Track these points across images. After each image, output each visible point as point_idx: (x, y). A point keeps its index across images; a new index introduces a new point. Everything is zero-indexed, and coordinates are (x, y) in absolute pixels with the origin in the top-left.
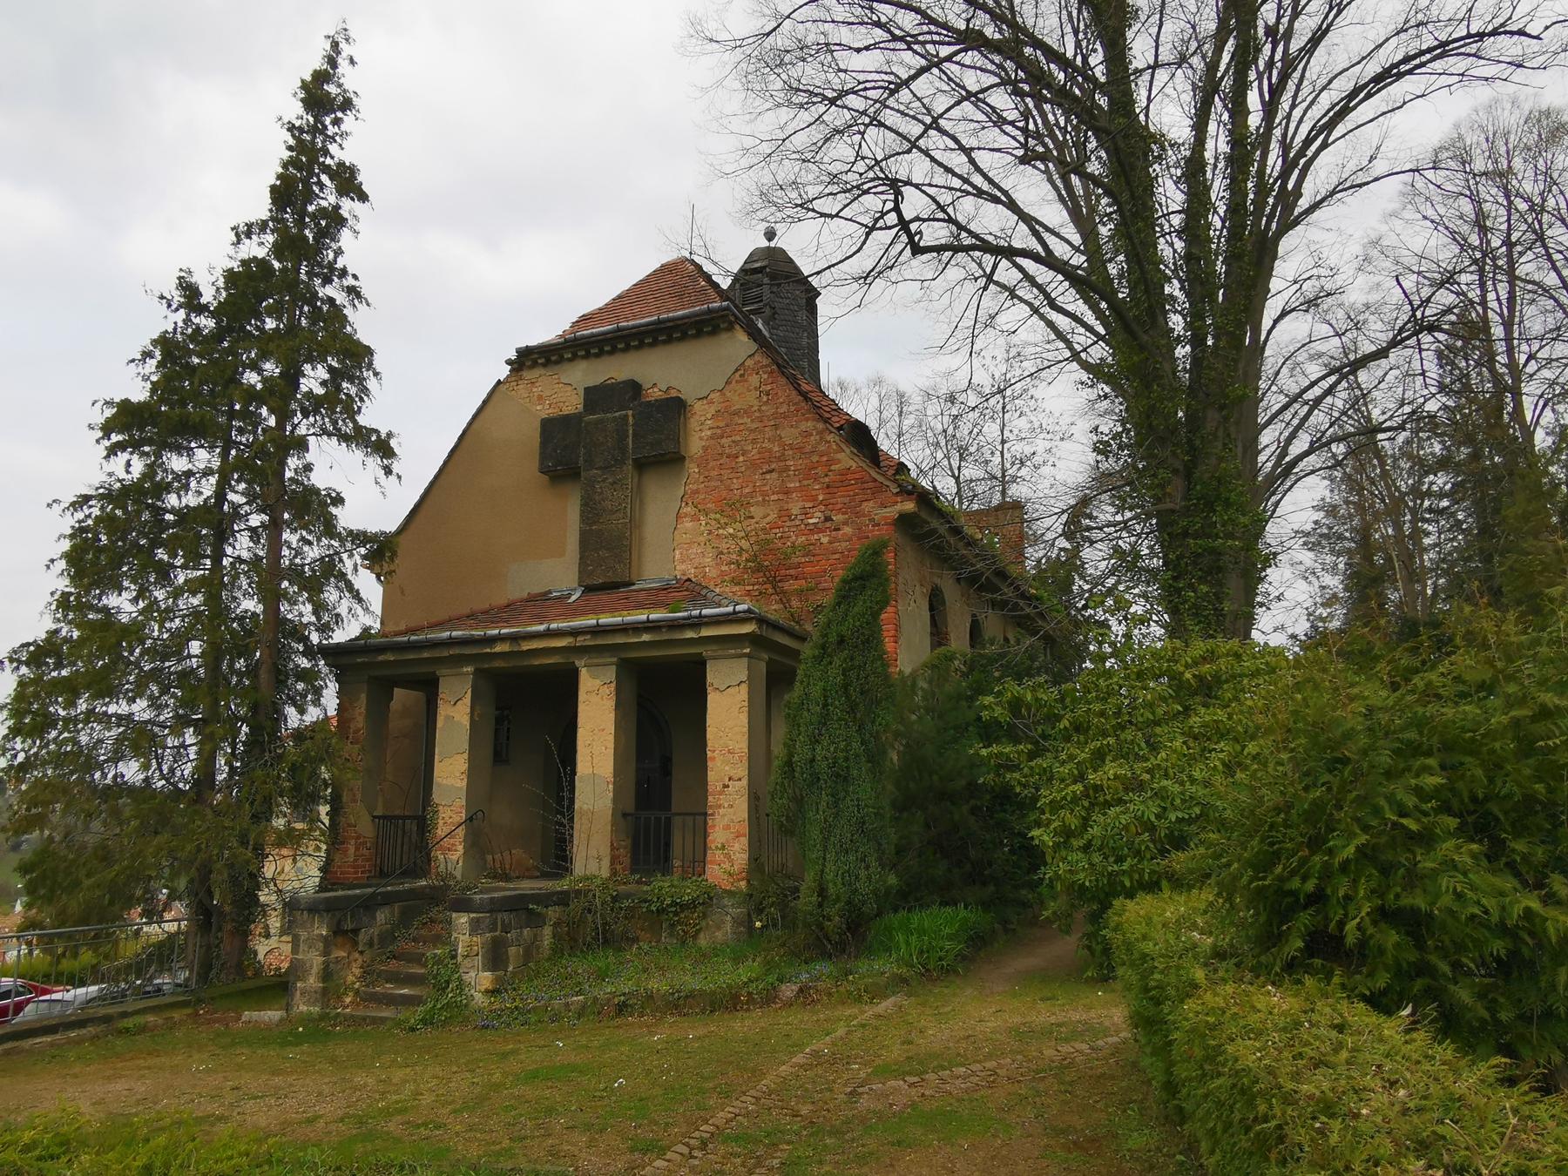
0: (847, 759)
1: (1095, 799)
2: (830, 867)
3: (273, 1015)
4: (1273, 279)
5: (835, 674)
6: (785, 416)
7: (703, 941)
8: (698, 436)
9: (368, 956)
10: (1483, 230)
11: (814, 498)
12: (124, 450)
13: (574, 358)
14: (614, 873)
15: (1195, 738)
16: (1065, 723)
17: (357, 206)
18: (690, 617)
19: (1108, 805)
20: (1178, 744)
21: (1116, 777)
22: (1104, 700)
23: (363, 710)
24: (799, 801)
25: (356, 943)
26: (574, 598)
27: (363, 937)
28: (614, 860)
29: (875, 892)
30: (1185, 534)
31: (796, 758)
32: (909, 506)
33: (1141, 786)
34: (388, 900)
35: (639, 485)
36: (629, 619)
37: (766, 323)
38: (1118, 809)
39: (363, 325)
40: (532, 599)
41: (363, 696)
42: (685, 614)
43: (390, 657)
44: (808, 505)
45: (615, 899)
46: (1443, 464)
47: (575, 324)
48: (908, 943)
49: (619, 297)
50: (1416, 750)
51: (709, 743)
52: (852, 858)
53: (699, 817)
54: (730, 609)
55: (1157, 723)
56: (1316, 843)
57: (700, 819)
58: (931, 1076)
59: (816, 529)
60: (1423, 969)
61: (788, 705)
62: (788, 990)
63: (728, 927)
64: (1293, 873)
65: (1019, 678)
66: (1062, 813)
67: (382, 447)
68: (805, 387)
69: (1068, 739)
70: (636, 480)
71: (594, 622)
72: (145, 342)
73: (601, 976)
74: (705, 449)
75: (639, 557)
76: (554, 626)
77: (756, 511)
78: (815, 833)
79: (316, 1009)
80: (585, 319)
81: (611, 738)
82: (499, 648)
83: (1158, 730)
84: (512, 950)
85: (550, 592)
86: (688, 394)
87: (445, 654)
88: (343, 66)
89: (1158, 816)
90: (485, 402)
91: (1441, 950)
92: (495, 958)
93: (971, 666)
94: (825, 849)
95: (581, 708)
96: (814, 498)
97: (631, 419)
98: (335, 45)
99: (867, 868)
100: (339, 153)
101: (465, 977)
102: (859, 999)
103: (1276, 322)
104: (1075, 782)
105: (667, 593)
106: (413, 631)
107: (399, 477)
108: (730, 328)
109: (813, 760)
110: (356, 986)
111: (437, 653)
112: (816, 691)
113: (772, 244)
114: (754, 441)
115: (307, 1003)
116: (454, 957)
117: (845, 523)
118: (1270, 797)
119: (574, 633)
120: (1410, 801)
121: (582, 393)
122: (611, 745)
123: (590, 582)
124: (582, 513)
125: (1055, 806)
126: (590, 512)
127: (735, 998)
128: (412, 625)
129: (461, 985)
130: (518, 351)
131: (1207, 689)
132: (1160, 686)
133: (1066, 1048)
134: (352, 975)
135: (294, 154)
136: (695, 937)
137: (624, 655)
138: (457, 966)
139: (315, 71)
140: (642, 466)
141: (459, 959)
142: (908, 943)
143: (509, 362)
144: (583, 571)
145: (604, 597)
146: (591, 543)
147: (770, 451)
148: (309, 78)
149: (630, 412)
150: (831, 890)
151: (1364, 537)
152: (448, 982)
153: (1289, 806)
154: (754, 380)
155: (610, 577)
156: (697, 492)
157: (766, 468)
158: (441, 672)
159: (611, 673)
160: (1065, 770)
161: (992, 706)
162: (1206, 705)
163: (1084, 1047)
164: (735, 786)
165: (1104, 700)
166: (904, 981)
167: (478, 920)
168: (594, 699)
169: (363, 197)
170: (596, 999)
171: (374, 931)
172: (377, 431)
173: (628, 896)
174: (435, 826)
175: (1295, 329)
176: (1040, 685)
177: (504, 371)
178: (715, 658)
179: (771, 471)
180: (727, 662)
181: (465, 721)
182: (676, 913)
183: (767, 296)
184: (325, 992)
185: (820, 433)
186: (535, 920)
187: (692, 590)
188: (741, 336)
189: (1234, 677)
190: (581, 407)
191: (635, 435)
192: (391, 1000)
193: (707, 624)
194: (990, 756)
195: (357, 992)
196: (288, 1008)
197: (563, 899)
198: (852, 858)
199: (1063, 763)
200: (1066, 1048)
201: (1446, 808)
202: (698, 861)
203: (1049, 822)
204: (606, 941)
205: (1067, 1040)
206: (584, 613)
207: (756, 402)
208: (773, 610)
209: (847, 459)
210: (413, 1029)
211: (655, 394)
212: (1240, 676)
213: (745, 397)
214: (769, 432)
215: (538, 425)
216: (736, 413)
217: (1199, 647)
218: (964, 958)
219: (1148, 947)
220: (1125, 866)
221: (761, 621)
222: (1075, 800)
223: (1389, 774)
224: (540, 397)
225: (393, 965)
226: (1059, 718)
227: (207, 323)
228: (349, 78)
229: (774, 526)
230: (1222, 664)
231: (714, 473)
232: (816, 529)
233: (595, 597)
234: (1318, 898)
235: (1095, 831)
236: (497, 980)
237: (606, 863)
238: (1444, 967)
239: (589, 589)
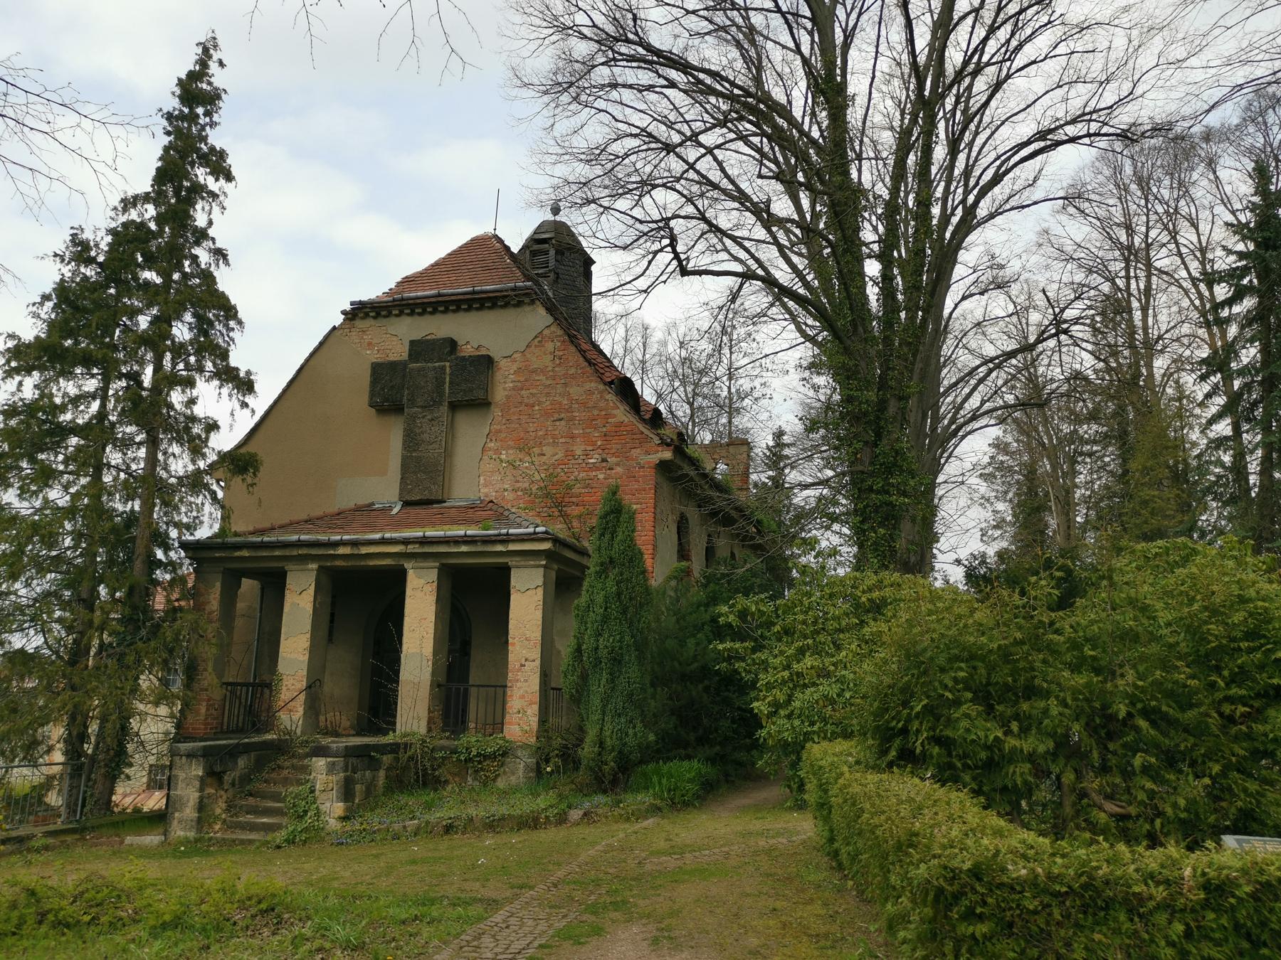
0: (621, 648)
1: (797, 682)
2: (608, 727)
4: (958, 267)
5: (611, 587)
6: (573, 377)
7: (501, 783)
8: (503, 386)
9: (231, 792)
10: (1129, 228)
11: (594, 444)
12: (18, 374)
13: (401, 314)
14: (429, 730)
15: (867, 643)
16: (777, 628)
17: (229, 187)
18: (499, 535)
19: (805, 686)
20: (853, 647)
21: (812, 667)
22: (806, 612)
23: (218, 595)
24: (584, 677)
26: (395, 511)
27: (227, 778)
28: (430, 721)
29: (639, 745)
30: (871, 490)
31: (584, 647)
32: (667, 455)
33: (828, 675)
34: (247, 749)
35: (452, 423)
36: (449, 533)
38: (813, 689)
40: (358, 509)
41: (218, 584)
42: (496, 532)
43: (245, 553)
45: (433, 750)
46: (1093, 417)
47: (399, 284)
48: (660, 783)
50: (957, 658)
51: (511, 632)
52: (623, 720)
53: (499, 690)
54: (531, 530)
55: (841, 631)
56: (905, 704)
57: (500, 690)
58: (687, 855)
59: (594, 468)
60: (951, 766)
61: (578, 607)
62: (575, 814)
63: (521, 773)
64: (893, 718)
65: (746, 595)
66: (774, 691)
67: (245, 385)
68: (584, 346)
69: (779, 640)
71: (421, 534)
72: (48, 288)
73: (428, 807)
74: (508, 397)
75: (450, 480)
76: (387, 535)
77: (548, 450)
78: (596, 701)
79: (192, 834)
80: (407, 281)
81: (432, 626)
82: (342, 551)
83: (841, 636)
84: (358, 787)
87: (295, 553)
88: (213, 67)
89: (838, 695)
90: (321, 344)
91: (960, 758)
92: (347, 793)
93: (709, 579)
94: (604, 713)
95: (408, 601)
96: (594, 444)
97: (448, 370)
98: (206, 50)
99: (634, 727)
100: (216, 138)
101: (321, 807)
102: (628, 819)
103: (1012, 209)
104: (784, 669)
105: (472, 511)
106: (262, 532)
108: (533, 302)
109: (597, 648)
110: (224, 816)
111: (287, 552)
112: (599, 598)
113: (558, 218)
114: (548, 394)
115: (184, 829)
116: (312, 791)
117: (618, 465)
118: (887, 680)
119: (406, 542)
120: (950, 684)
121: (407, 345)
122: (432, 631)
123: (408, 498)
124: (404, 442)
125: (770, 687)
126: (411, 441)
127: (536, 820)
128: (259, 526)
129: (318, 814)
130: (352, 304)
131: (877, 608)
132: (842, 606)
133: (771, 842)
134: (219, 808)
135: (172, 138)
136: (494, 780)
137: (444, 561)
139: (190, 72)
140: (454, 407)
141: (317, 793)
142: (660, 783)
143: (344, 312)
145: (421, 512)
146: (409, 466)
147: (560, 403)
148: (184, 77)
149: (448, 364)
150: (609, 742)
151: (1031, 473)
152: (306, 812)
153: (894, 685)
154: (550, 346)
155: (426, 495)
156: (500, 431)
157: (556, 416)
158: (289, 567)
159: (433, 575)
160: (777, 661)
161: (726, 613)
162: (875, 620)
163: (784, 841)
164: (529, 665)
165: (806, 612)
166: (659, 809)
167: (334, 763)
169: (229, 178)
170: (428, 823)
173: (442, 748)
174: (279, 692)
175: (974, 308)
176: (762, 600)
177: (339, 319)
178: (518, 567)
180: (527, 571)
181: (309, 608)
182: (480, 762)
183: (552, 263)
184: (199, 820)
185: (601, 392)
186: (374, 765)
187: (490, 510)
189: (895, 600)
190: (405, 356)
191: (451, 383)
192: (253, 827)
193: (513, 541)
194: (725, 649)
197: (394, 748)
198: (623, 720)
199: (776, 656)
200: (771, 842)
201: (967, 688)
202: (498, 725)
203: (766, 697)
204: (425, 784)
205: (773, 837)
206: (410, 526)
208: (559, 529)
209: (621, 413)
210: (279, 847)
211: (467, 351)
212: (900, 600)
213: (542, 359)
214: (560, 389)
217: (871, 579)
218: (698, 797)
219: (823, 763)
220: (816, 728)
221: (556, 540)
222: (784, 682)
223: (943, 670)
225: (251, 800)
226: (774, 624)
227: (90, 272)
228: (219, 78)
229: (560, 463)
230: (887, 592)
232: (594, 468)
233: (413, 511)
234: (904, 731)
235: (797, 704)
236: (347, 809)
237: (424, 723)
238: (959, 765)
239: (407, 504)
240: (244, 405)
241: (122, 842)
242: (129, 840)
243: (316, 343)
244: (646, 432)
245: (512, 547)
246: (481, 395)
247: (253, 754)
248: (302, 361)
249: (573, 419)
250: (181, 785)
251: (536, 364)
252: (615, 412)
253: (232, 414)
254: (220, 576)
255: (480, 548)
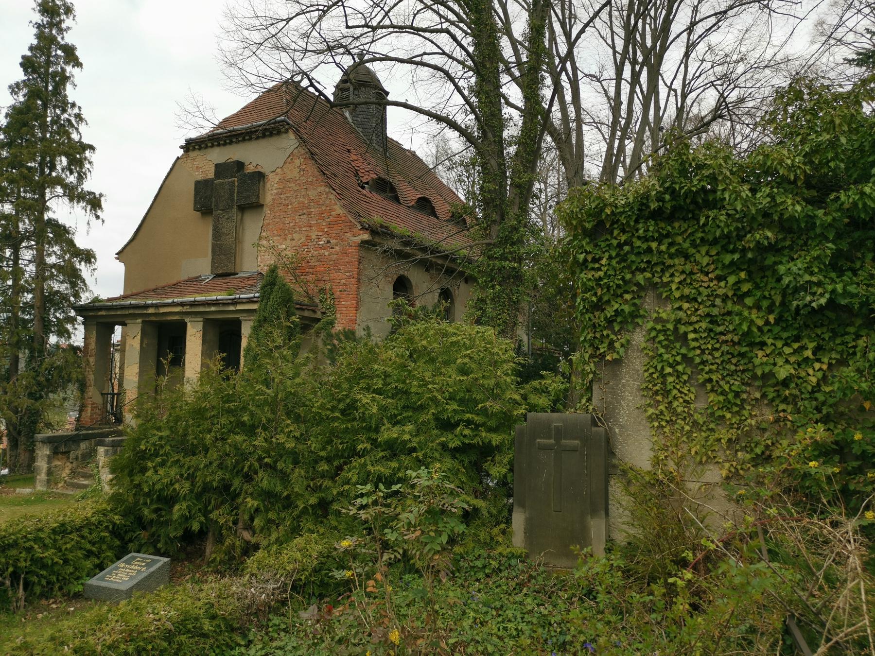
3: (28, 490)
8: (270, 193)
25: (68, 458)
27: (72, 455)
32: (366, 236)
35: (242, 219)
36: (209, 298)
37: (351, 113)
39: (86, 134)
40: (189, 280)
41: (95, 332)
43: (103, 313)
44: (320, 234)
49: (245, 107)
59: (322, 248)
67: (94, 203)
70: (239, 217)
74: (273, 200)
85: (200, 276)
86: (265, 170)
90: (171, 169)
95: (188, 343)
97: (236, 183)
100: (69, 39)
101: (102, 477)
107: (103, 221)
108: (286, 132)
114: (296, 197)
117: (336, 245)
119: (182, 304)
126: (217, 234)
130: (186, 141)
134: (65, 473)
138: (98, 471)
140: (242, 209)
143: (181, 147)
144: (213, 267)
154: (297, 162)
156: (269, 224)
157: (301, 212)
159: (200, 326)
168: (193, 339)
171: (79, 453)
172: (94, 193)
178: (245, 321)
179: (304, 214)
185: (327, 194)
188: (291, 135)
190: (211, 175)
193: (239, 303)
195: (65, 482)
196: (34, 487)
207: (298, 175)
211: (250, 169)
214: (303, 192)
215: (193, 187)
216: (288, 181)
224: (197, 168)
231: (277, 214)
232: (322, 248)
233: (220, 281)
240: (98, 217)
241: (15, 491)
242: (18, 490)
243: (168, 170)
244: (353, 221)
245: (239, 307)
246: (254, 200)
247: (93, 441)
248: (161, 182)
249: (310, 213)
250: (40, 459)
251: (289, 176)
252: (335, 207)
253: (88, 224)
254: (95, 327)
255: (221, 309)
